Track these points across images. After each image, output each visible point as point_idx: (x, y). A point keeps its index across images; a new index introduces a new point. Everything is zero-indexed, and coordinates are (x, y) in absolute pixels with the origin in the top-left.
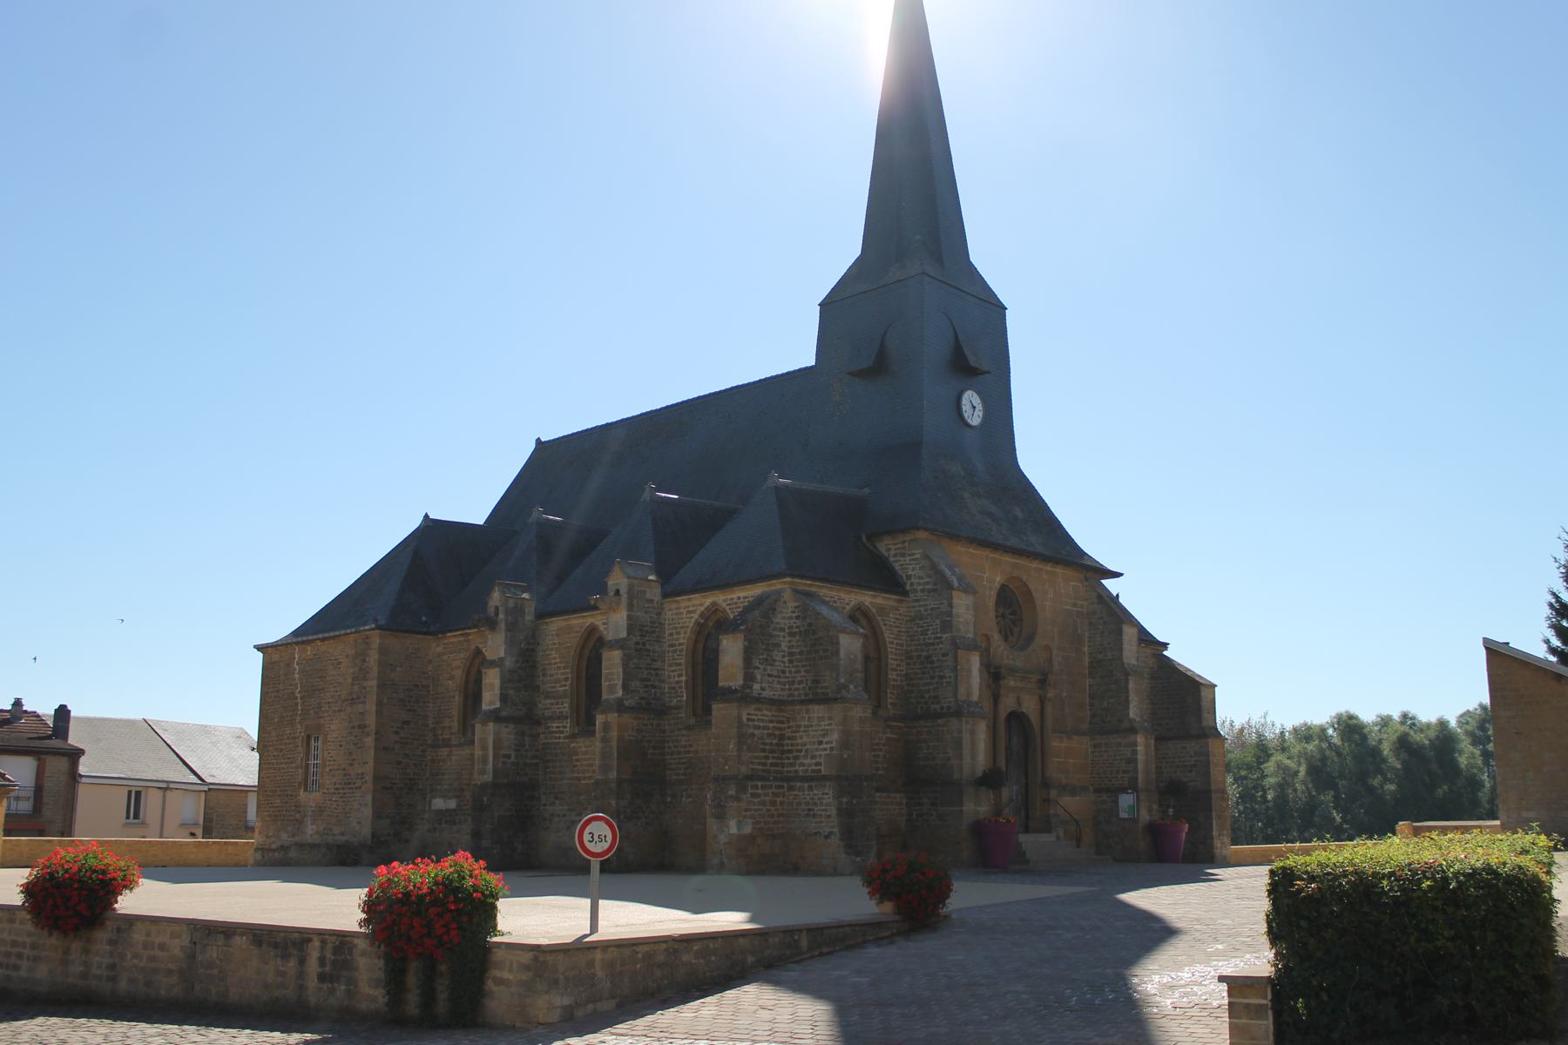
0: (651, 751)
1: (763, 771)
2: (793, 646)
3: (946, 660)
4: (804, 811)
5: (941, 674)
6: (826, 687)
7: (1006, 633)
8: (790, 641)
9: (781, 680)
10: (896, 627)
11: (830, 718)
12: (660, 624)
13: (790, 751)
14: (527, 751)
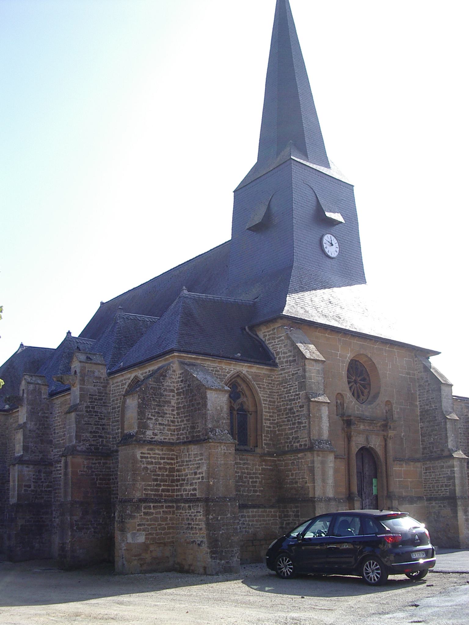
0: (99, 481)
1: (155, 495)
2: (179, 403)
3: (302, 411)
4: (186, 525)
5: (300, 420)
6: (199, 432)
7: (358, 393)
8: (178, 399)
9: (171, 428)
10: (269, 389)
11: (201, 454)
12: (106, 393)
13: (178, 480)
14: (42, 482)
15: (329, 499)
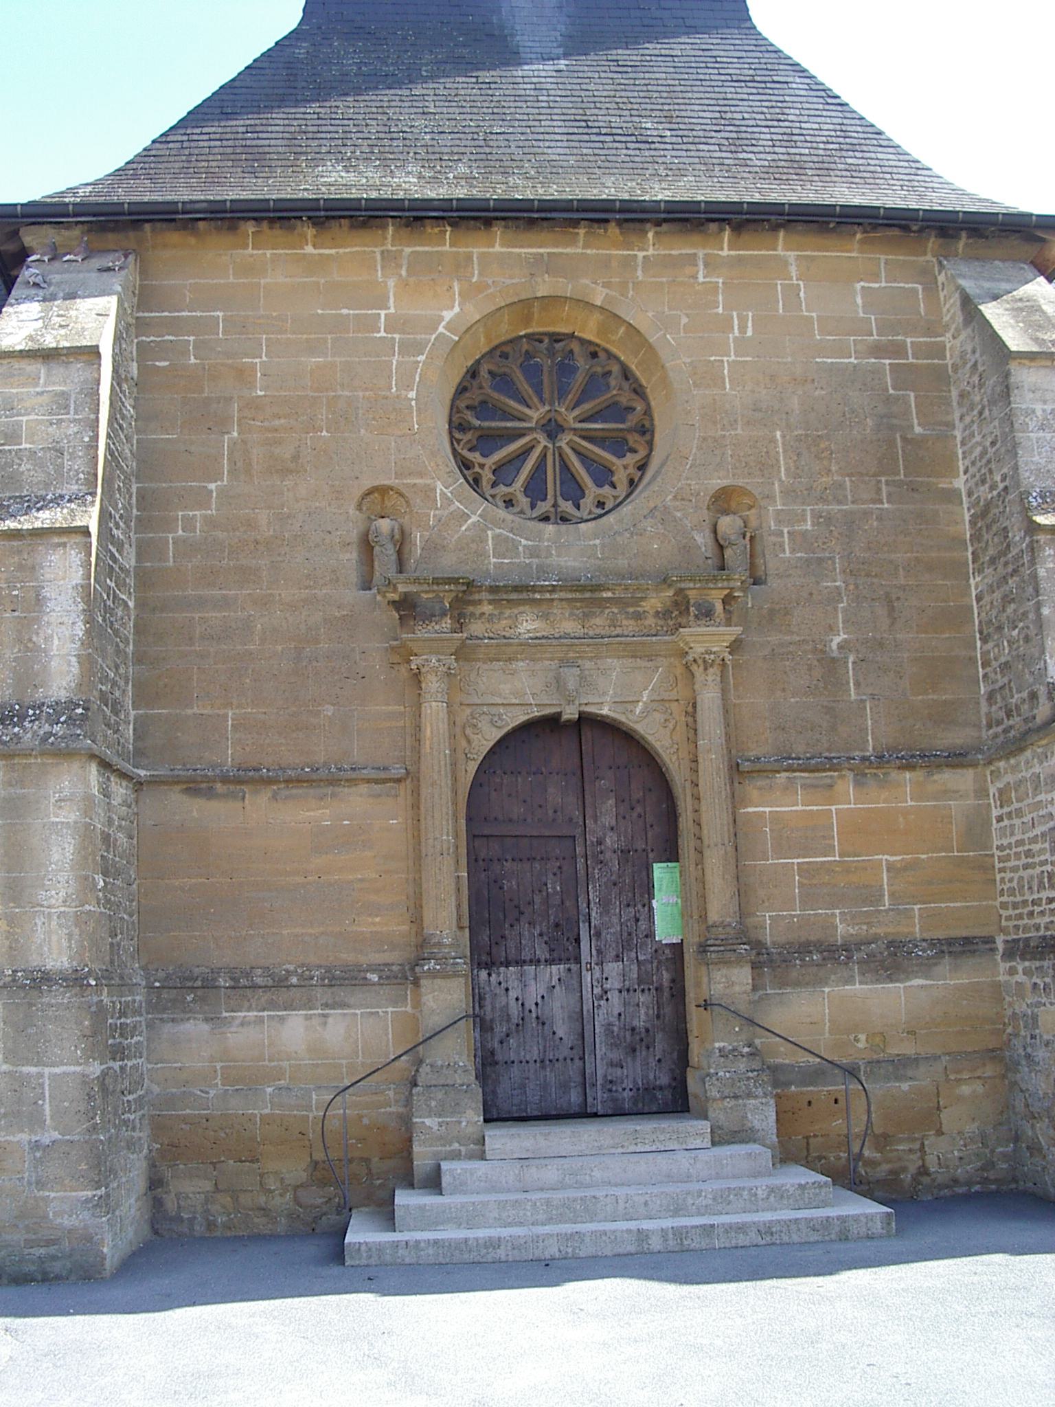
15: (42, 980)
